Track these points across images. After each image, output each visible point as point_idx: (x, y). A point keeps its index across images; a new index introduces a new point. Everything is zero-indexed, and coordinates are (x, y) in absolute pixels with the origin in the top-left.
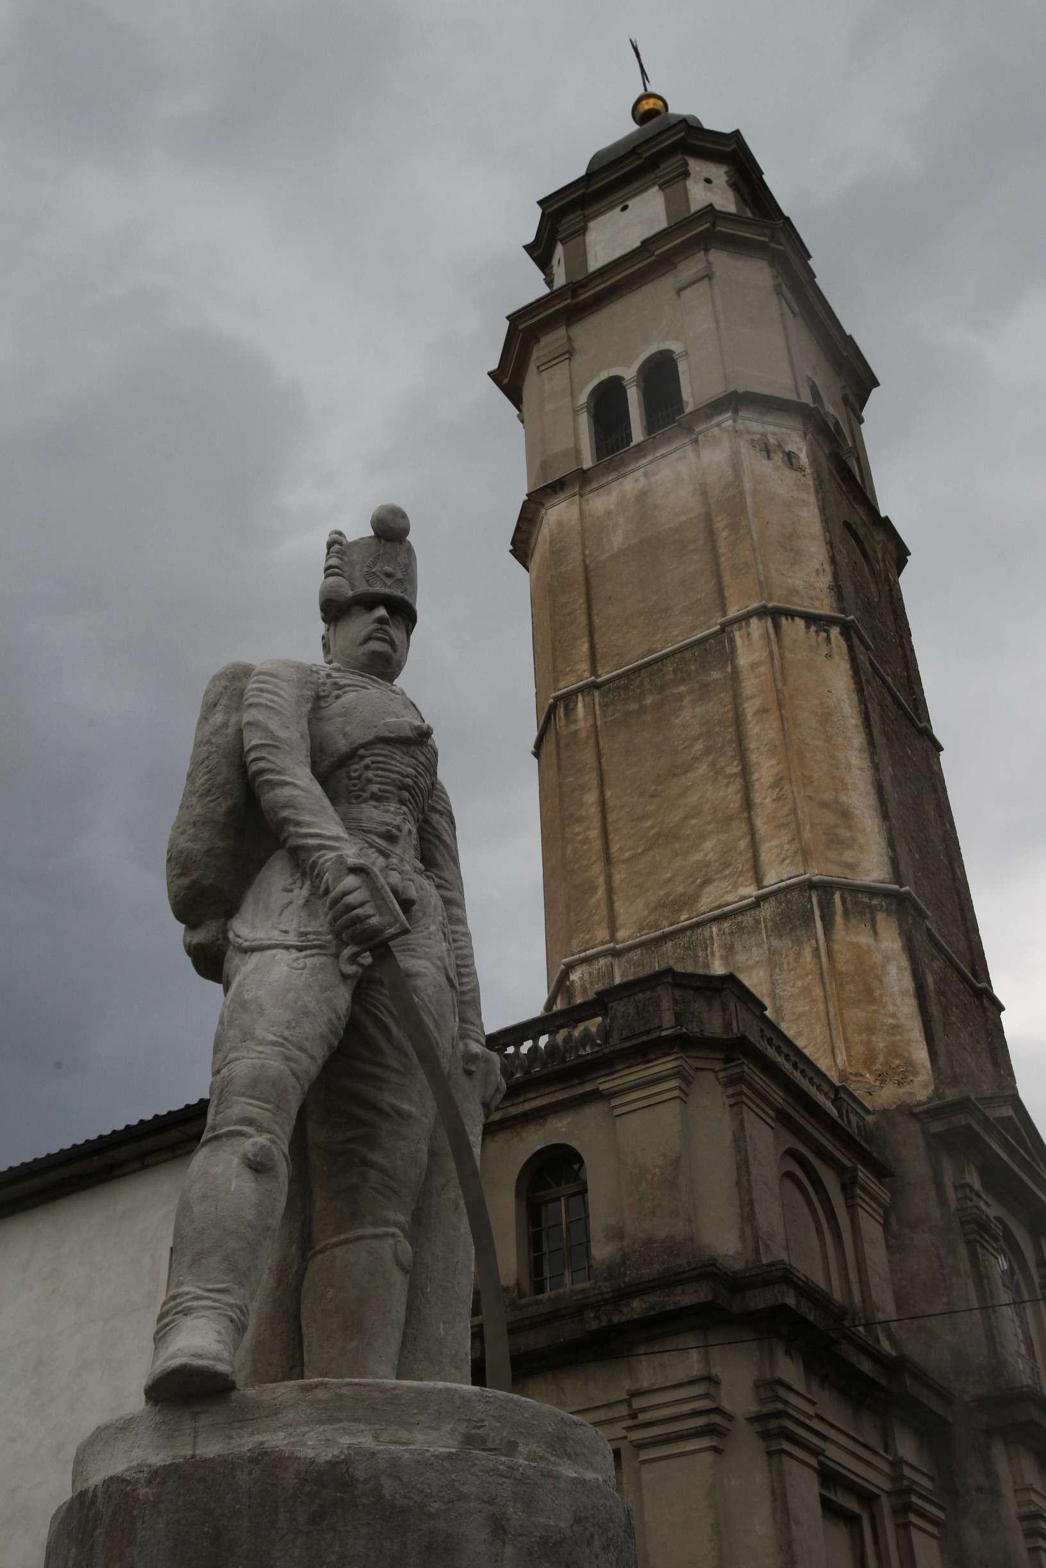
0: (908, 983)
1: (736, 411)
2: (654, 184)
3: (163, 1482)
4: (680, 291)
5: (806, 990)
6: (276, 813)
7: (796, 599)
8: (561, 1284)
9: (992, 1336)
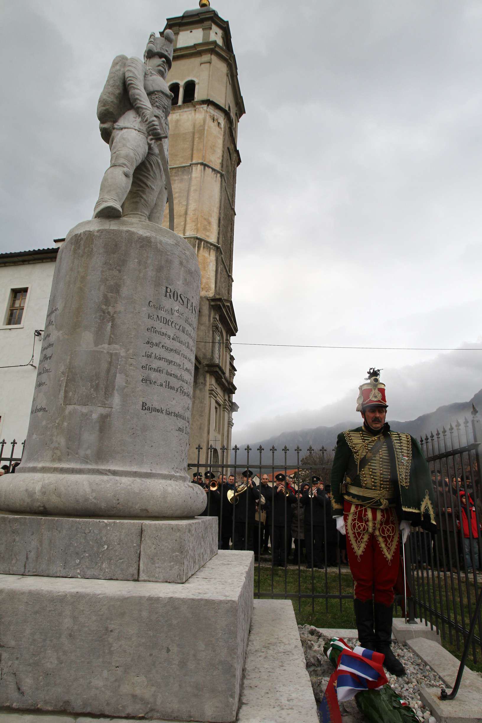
0: (214, 269)
1: (208, 105)
2: (201, 28)
4: (201, 64)
6: (134, 96)
7: (211, 163)
9: (213, 352)
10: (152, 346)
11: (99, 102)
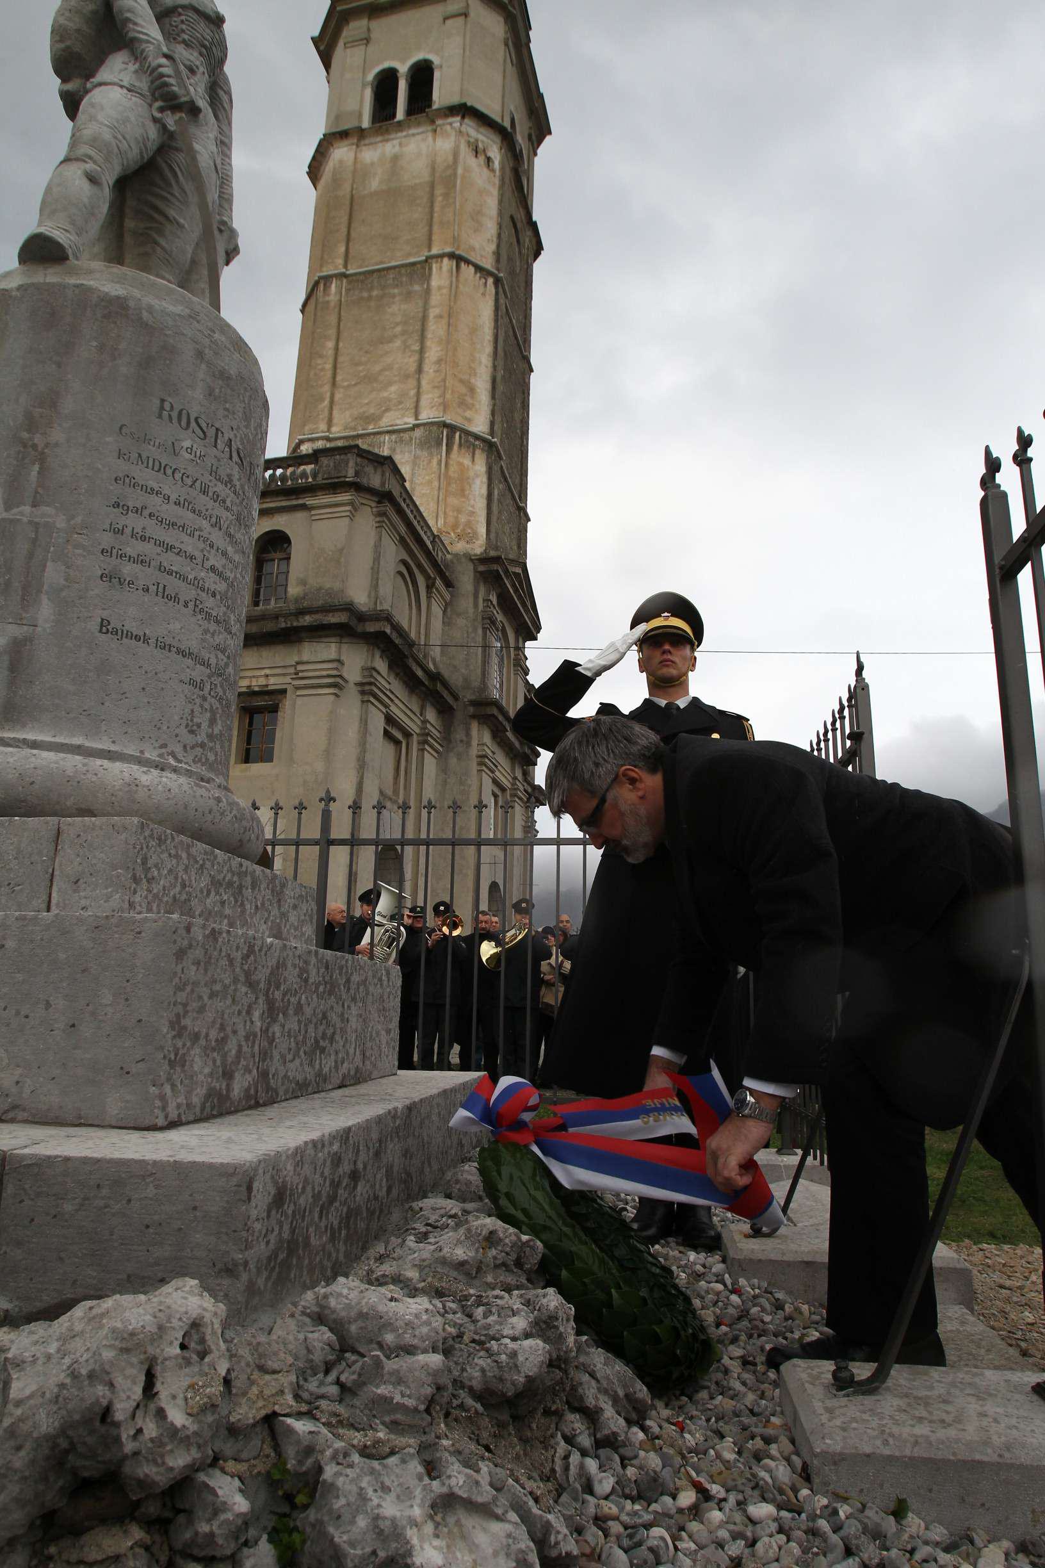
0: (484, 491)
1: (463, 117)
3: (26, 290)
4: (445, 19)
5: (430, 482)
6: (122, 14)
7: (472, 253)
8: (269, 604)
9: (484, 674)
10: (124, 512)
11: (52, 32)
